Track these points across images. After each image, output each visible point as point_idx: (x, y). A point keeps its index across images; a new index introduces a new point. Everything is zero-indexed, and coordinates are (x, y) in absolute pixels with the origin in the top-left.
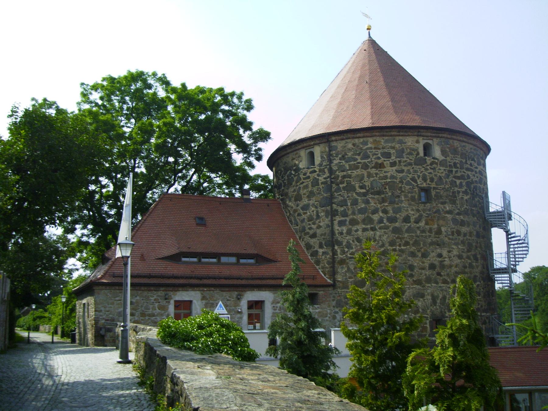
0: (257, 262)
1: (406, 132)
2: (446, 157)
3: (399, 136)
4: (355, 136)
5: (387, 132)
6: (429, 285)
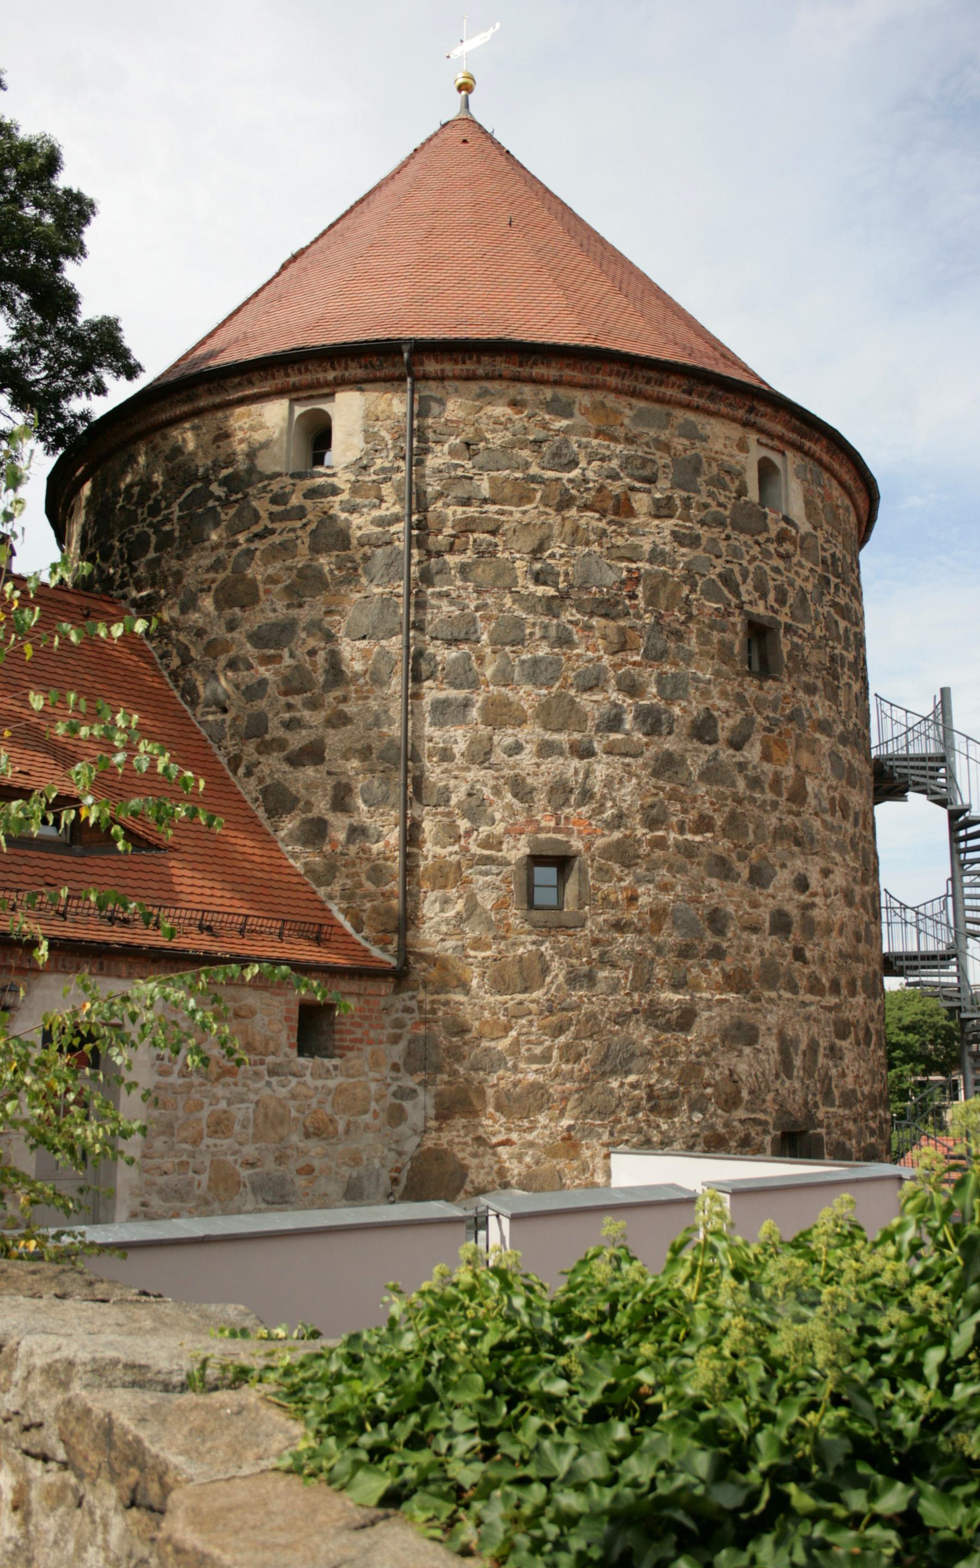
1: (712, 397)
2: (815, 528)
3: (687, 406)
4: (525, 371)
5: (648, 382)
6: (773, 994)
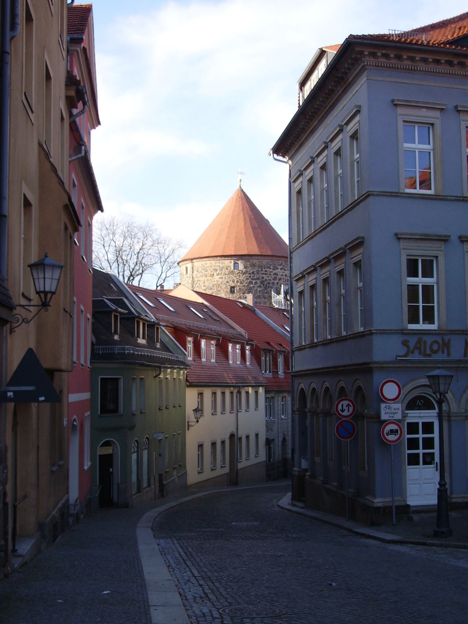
0: (83, 145)
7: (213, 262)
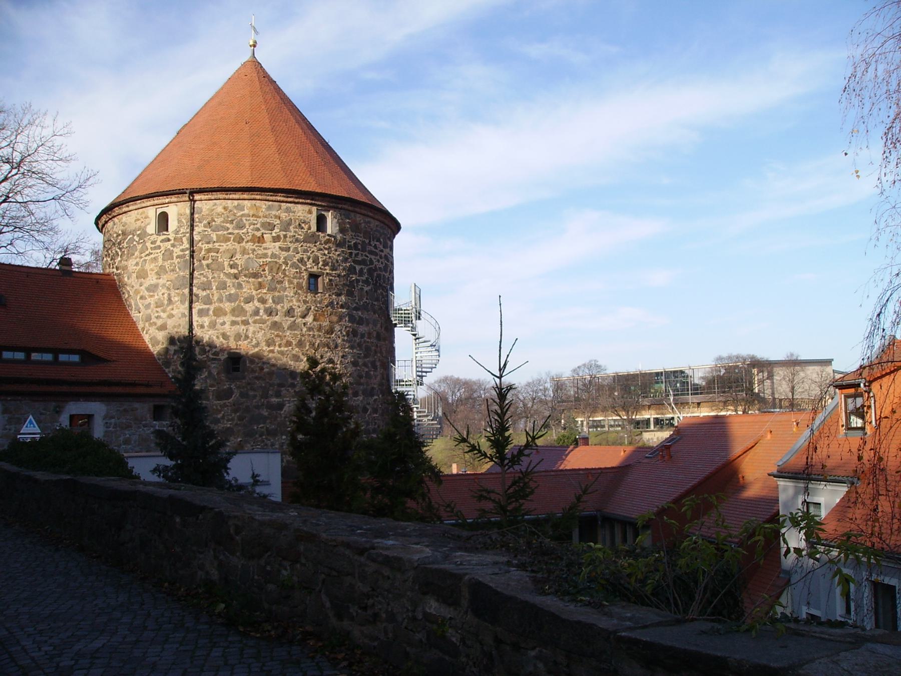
3: (287, 202)
7: (263, 205)
